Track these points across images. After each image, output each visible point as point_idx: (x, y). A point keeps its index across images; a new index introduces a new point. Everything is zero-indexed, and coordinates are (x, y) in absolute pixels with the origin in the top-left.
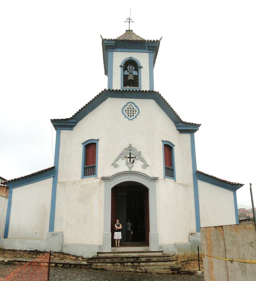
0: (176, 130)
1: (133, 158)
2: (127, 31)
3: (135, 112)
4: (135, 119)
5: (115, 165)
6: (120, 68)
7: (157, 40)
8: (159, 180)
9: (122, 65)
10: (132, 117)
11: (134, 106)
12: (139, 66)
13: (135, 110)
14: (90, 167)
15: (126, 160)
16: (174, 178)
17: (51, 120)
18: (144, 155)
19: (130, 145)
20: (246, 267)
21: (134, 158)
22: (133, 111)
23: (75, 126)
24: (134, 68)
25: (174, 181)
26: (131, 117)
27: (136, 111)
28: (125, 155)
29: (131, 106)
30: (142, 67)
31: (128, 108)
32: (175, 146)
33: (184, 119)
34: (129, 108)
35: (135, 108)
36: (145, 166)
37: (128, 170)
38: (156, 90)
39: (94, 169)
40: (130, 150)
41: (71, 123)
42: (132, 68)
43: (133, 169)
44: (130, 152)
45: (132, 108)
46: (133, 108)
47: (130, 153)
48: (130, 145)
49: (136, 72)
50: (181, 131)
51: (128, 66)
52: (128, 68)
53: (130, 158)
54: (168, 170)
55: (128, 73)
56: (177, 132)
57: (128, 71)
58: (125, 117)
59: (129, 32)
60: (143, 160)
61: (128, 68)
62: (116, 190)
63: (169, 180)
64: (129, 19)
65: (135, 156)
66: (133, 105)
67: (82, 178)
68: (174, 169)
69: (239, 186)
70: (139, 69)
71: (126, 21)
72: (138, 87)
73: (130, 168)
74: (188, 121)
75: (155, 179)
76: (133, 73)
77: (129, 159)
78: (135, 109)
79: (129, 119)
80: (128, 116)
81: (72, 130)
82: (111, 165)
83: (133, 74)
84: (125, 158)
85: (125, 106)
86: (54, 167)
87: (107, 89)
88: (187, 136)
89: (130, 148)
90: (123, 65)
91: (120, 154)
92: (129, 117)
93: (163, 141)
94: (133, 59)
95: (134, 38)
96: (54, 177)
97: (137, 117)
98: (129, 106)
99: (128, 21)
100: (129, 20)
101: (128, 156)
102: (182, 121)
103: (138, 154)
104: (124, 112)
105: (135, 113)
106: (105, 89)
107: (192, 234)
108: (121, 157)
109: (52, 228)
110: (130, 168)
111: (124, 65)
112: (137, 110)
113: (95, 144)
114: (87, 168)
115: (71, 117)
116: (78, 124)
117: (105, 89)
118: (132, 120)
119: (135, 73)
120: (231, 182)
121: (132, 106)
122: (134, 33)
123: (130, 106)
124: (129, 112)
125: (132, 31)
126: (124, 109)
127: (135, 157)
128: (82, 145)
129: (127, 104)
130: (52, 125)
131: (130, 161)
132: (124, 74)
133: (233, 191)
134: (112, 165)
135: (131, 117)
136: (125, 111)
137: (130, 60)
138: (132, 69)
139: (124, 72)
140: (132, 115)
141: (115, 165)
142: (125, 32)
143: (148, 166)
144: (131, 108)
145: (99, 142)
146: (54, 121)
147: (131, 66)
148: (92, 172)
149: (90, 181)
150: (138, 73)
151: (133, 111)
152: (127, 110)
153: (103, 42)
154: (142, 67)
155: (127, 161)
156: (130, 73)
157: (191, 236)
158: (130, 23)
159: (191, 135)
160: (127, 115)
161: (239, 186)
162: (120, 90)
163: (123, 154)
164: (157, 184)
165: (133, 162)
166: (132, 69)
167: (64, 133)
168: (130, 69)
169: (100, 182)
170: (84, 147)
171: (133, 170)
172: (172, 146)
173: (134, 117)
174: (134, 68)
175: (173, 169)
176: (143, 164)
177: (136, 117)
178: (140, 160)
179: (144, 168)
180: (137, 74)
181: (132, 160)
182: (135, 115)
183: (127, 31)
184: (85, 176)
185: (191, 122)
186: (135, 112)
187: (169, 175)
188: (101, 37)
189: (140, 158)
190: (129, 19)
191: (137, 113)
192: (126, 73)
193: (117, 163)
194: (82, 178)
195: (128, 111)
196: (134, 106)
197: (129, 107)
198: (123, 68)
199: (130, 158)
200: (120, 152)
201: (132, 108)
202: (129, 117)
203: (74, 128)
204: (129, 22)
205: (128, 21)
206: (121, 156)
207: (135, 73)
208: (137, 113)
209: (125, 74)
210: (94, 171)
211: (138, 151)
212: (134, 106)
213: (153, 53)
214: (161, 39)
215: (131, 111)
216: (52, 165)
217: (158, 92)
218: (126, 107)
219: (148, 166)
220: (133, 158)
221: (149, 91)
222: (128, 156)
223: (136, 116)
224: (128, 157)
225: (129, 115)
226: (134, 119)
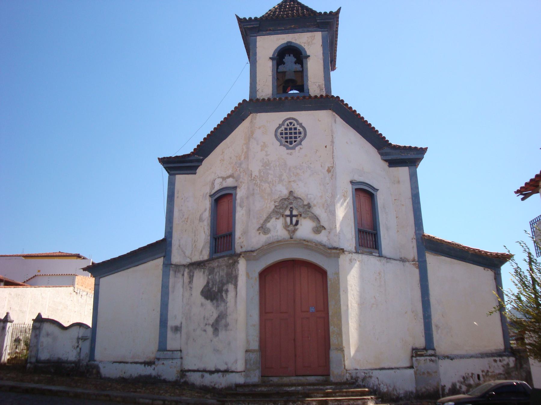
1: (296, 216)
6: (308, 53)
10: (294, 144)
11: (297, 125)
14: (221, 238)
17: (159, 159)
20: (356, 369)
21: (299, 216)
29: (291, 125)
30: (309, 56)
31: (286, 129)
32: (378, 190)
33: (394, 140)
34: (288, 129)
38: (334, 93)
41: (191, 161)
45: (293, 127)
47: (291, 208)
50: (392, 163)
53: (291, 216)
56: (386, 165)
60: (316, 219)
68: (378, 233)
69: (504, 258)
70: (304, 60)
74: (402, 144)
77: (288, 219)
78: (299, 130)
80: (287, 142)
81: (195, 174)
84: (283, 216)
87: (248, 99)
88: (403, 172)
92: (288, 144)
94: (292, 45)
96: (164, 257)
98: (288, 125)
102: (391, 144)
113: (231, 195)
115: (192, 152)
116: (204, 162)
120: (499, 252)
121: (294, 125)
123: (289, 124)
133: (491, 270)
139: (277, 68)
141: (263, 229)
144: (291, 129)
146: (164, 161)
150: (302, 67)
154: (309, 56)
155: (286, 222)
160: (284, 140)
161: (504, 258)
165: (297, 223)
167: (181, 179)
170: (213, 201)
175: (377, 233)
180: (301, 70)
181: (294, 219)
185: (407, 145)
191: (302, 135)
193: (269, 225)
196: (297, 125)
197: (288, 127)
198: (275, 62)
199: (291, 216)
203: (200, 170)
209: (279, 71)
216: (160, 235)
218: (283, 128)
220: (296, 216)
223: (301, 141)
224: (287, 216)
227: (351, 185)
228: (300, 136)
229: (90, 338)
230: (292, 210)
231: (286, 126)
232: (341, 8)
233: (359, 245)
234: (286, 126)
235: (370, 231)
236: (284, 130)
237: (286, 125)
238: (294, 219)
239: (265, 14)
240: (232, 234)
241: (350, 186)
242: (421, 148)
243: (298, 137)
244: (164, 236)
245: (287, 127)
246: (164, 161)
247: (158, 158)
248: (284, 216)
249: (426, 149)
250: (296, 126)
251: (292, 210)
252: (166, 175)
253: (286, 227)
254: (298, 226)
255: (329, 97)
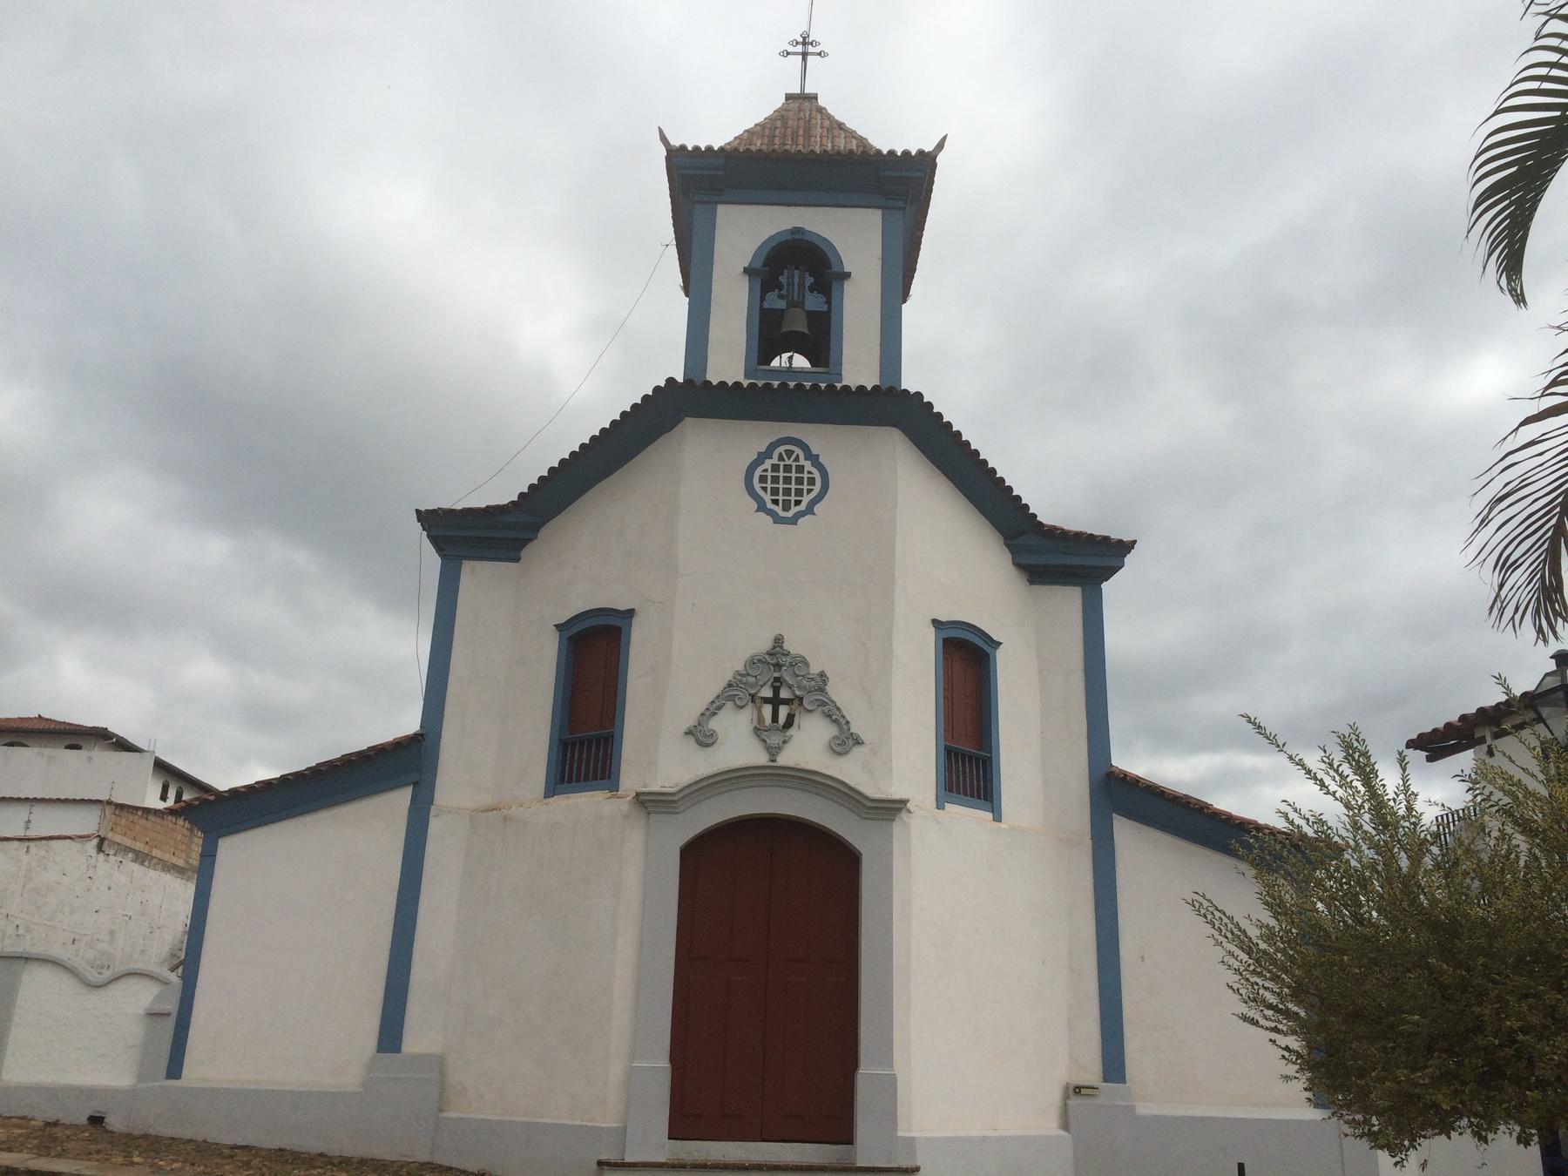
0: (1012, 566)
1: (787, 702)
2: (789, 97)
3: (805, 487)
4: (808, 517)
5: (701, 736)
7: (921, 152)
8: (909, 811)
9: (754, 266)
12: (835, 269)
13: (806, 475)
14: (582, 744)
15: (755, 713)
16: (992, 802)
17: (418, 511)
18: (838, 691)
19: (778, 641)
21: (796, 703)
22: (799, 481)
23: (530, 540)
24: (809, 280)
25: (990, 815)
26: (786, 508)
27: (812, 481)
28: (752, 686)
29: (789, 459)
30: (848, 275)
31: (775, 468)
35: (808, 465)
36: (845, 742)
37: (761, 758)
38: (909, 383)
39: (605, 755)
40: (778, 666)
42: (802, 279)
43: (786, 758)
44: (777, 675)
45: (794, 464)
46: (800, 469)
47: (777, 679)
48: (778, 641)
49: (822, 299)
51: (786, 272)
52: (783, 279)
53: (776, 702)
54: (963, 762)
55: (782, 305)
57: (784, 292)
58: (762, 507)
59: (802, 102)
60: (834, 715)
61: (783, 279)
62: (697, 855)
63: (965, 818)
64: (804, 43)
65: (798, 693)
66: (798, 451)
67: (550, 792)
70: (835, 285)
71: (791, 49)
72: (827, 365)
73: (773, 752)
75: (891, 809)
76: (803, 303)
77: (767, 710)
78: (809, 472)
79: (778, 520)
80: (775, 502)
81: (517, 560)
82: (686, 733)
83: (806, 308)
84: (753, 701)
85: (762, 457)
86: (422, 735)
87: (680, 379)
88: (1069, 599)
89: (776, 658)
90: (758, 265)
91: (730, 685)
93: (936, 623)
95: (820, 143)
96: (416, 784)
97: (816, 509)
98: (781, 458)
99: (799, 48)
100: (805, 47)
101: (767, 692)
103: (813, 683)
104: (757, 486)
105: (809, 491)
106: (671, 381)
107: (1078, 1090)
108: (731, 698)
109: (390, 1035)
110: (773, 752)
111: (764, 265)
112: (817, 475)
114: (574, 744)
115: (512, 502)
117: (671, 381)
118: (793, 521)
119: (814, 302)
121: (797, 459)
122: (821, 110)
124: (781, 486)
125: (814, 97)
126: (758, 472)
127: (801, 699)
128: (557, 635)
129: (773, 446)
130: (425, 533)
131: (775, 718)
132: (761, 306)
134: (689, 733)
135: (786, 508)
136: (763, 479)
137: (794, 240)
138: (799, 284)
139: (763, 299)
140: (793, 498)
141: (701, 736)
142: (779, 101)
143: (858, 742)
144: (788, 468)
145: (637, 624)
146: (432, 520)
147: (796, 272)
148: (579, 769)
149: (588, 803)
150: (829, 302)
151: (799, 481)
152: (769, 474)
153: (668, 159)
154: (848, 275)
155: (761, 719)
156: (792, 304)
157: (1074, 1101)
158: (809, 58)
159: (1083, 590)
160: (767, 498)
162: (737, 385)
163: (745, 684)
164: (897, 827)
166: (801, 285)
167: (478, 577)
168: (793, 284)
169: (626, 817)
171: (785, 759)
172: (985, 647)
173: (803, 507)
174: (812, 280)
176: (837, 734)
177: (810, 510)
178: (823, 712)
179: (835, 752)
180: (825, 308)
181: (783, 712)
182: (806, 499)
183: (789, 97)
184: (562, 782)
186: (805, 487)
187: (979, 790)
188: (664, 139)
189: (824, 704)
190: (804, 43)
192: (774, 302)
193: (714, 724)
194: (550, 792)
195: (775, 480)
196: (806, 459)
197: (782, 464)
199: (776, 702)
200: (729, 676)
201: (794, 464)
202: (778, 509)
204: (804, 55)
205: (799, 48)
206: (735, 692)
207: (814, 302)
208: (817, 488)
209: (766, 305)
210: (604, 762)
211: (815, 669)
212: (802, 457)
213: (901, 209)
214: (940, 146)
215: (787, 480)
216: (409, 722)
217: (919, 395)
218: (768, 464)
219: (858, 742)
220: (787, 702)
221: (875, 387)
222: (767, 692)
224: (766, 700)
225: (781, 498)
226: (801, 521)
227: (933, 630)
228: (812, 490)
229: (175, 1014)
230: (777, 684)
231: (775, 460)
232: (947, 135)
233: (945, 790)
234: (775, 460)
235: (973, 751)
236: (769, 470)
237: (777, 456)
238: (783, 712)
239: (733, 139)
240: (613, 736)
241: (932, 630)
242: (1120, 541)
243: (805, 492)
244: (419, 725)
245: (778, 463)
246: (432, 520)
247: (417, 510)
248: (758, 701)
249: (1134, 542)
250: (802, 462)
251: (777, 684)
252: (432, 560)
253: (759, 731)
254: (792, 731)
255: (894, 392)
